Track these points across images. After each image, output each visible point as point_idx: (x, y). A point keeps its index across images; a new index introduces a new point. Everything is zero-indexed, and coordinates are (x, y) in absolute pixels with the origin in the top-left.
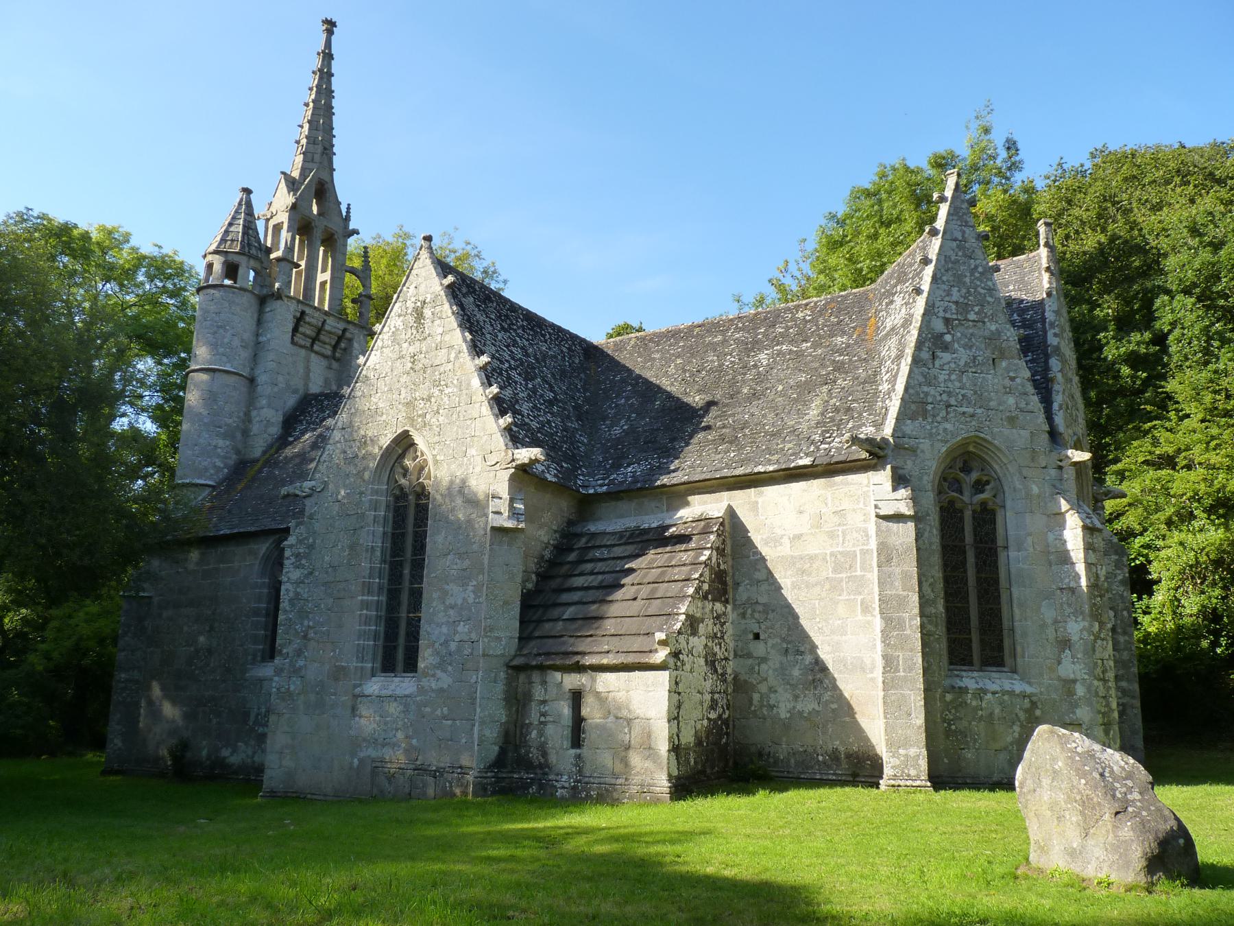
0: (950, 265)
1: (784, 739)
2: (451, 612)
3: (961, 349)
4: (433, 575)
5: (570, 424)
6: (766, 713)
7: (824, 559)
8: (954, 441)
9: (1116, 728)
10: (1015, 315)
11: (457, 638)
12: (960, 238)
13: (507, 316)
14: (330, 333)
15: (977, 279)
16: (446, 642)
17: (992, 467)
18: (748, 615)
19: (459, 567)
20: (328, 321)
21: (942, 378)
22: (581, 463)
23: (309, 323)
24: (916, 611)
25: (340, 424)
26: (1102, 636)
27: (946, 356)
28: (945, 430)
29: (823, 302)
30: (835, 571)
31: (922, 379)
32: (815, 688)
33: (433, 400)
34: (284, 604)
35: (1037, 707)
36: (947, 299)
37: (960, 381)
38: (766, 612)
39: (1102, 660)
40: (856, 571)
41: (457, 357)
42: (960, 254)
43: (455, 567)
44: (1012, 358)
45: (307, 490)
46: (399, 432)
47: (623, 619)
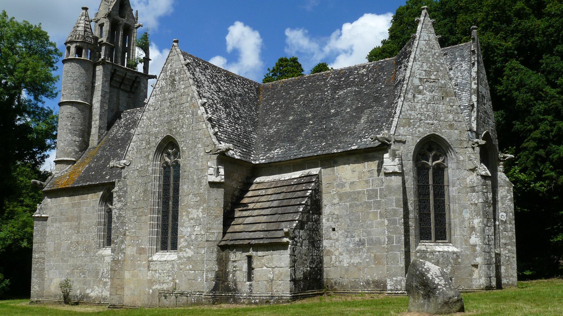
0: (423, 53)
1: (346, 276)
2: (192, 221)
3: (428, 93)
4: (183, 204)
5: (248, 129)
6: (338, 264)
7: (364, 193)
8: (423, 136)
9: (494, 265)
10: (459, 73)
11: (195, 233)
12: (428, 40)
13: (216, 76)
14: (129, 79)
15: (436, 59)
16: (190, 235)
17: (442, 148)
18: (330, 220)
19: (195, 200)
20: (128, 74)
21: (417, 107)
22: (253, 148)
23: (118, 75)
24: (402, 216)
25: (137, 133)
26: (489, 225)
27: (420, 97)
28: (419, 131)
29: (373, 65)
30: (368, 199)
31: (408, 108)
32: (359, 252)
33: (180, 121)
34: (114, 219)
35: (459, 258)
36: (421, 69)
37: (427, 108)
38: (338, 218)
39: (488, 235)
40: (378, 198)
41: (191, 100)
42: (427, 47)
43: (193, 200)
44: (452, 96)
45: (122, 164)
46: (165, 136)
47: (270, 221)
